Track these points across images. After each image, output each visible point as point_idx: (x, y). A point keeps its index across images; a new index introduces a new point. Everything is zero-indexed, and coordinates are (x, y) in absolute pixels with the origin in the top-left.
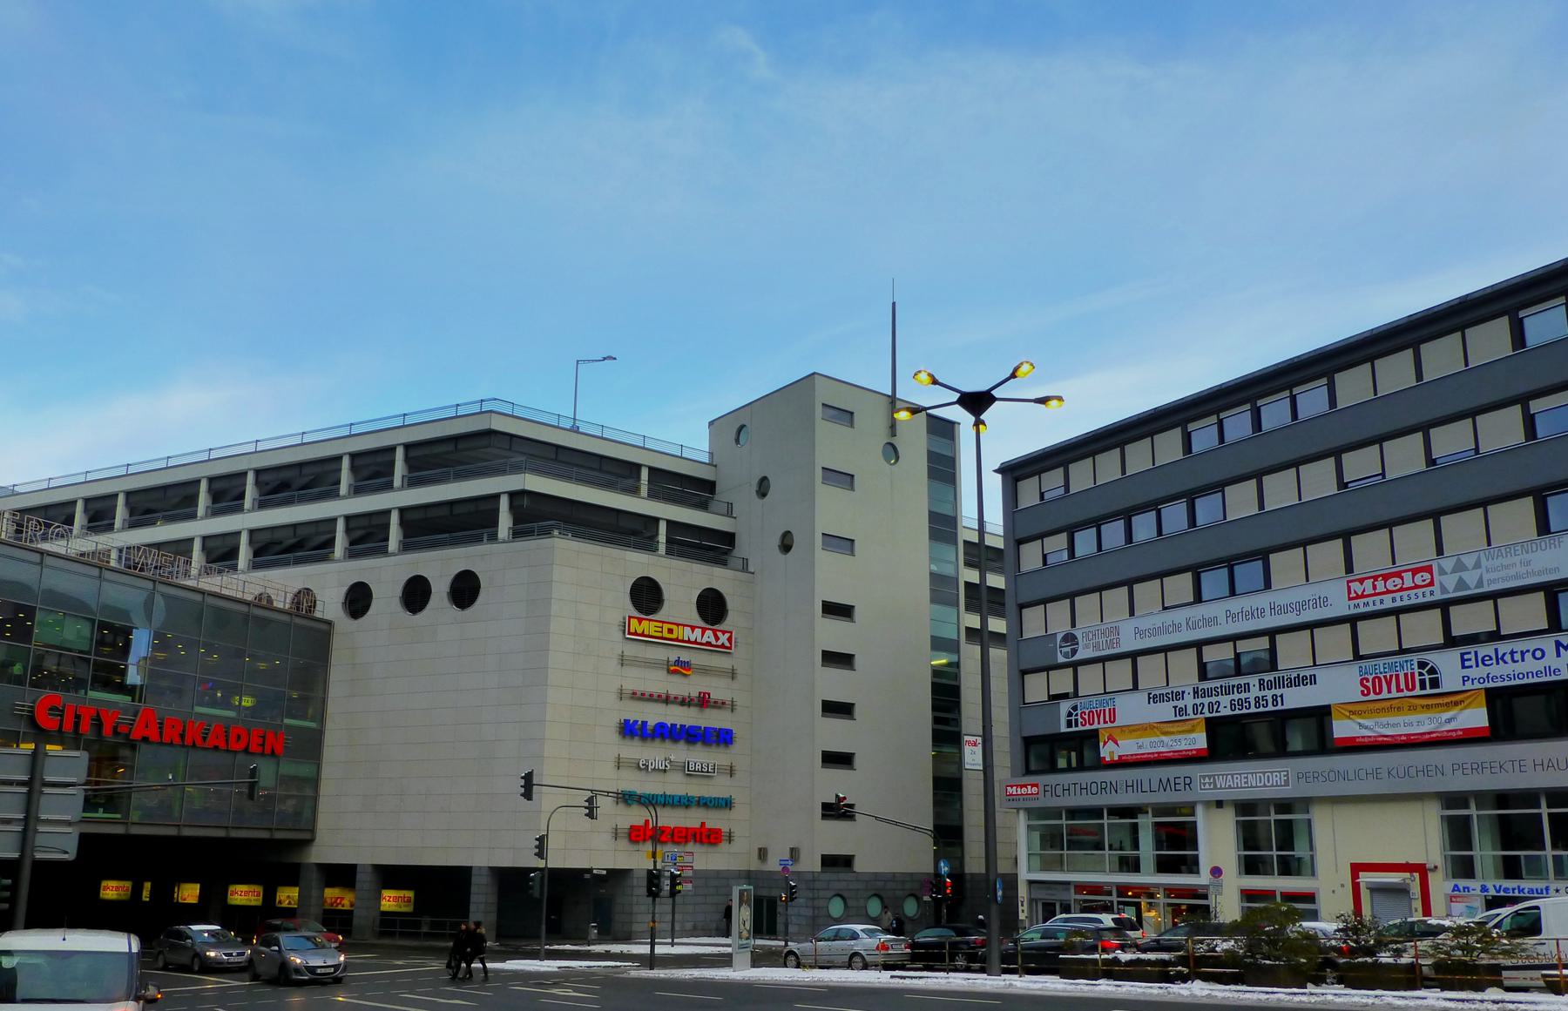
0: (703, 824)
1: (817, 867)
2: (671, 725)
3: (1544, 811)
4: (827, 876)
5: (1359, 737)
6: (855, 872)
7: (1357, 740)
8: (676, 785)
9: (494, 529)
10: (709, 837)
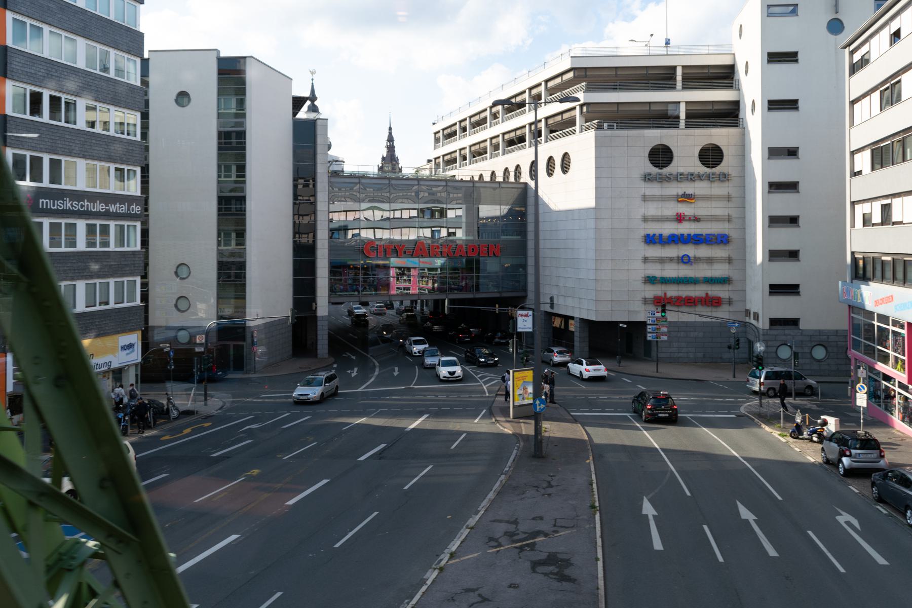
0: (707, 294)
1: (767, 326)
2: (688, 235)
3: (487, 395)
4: (774, 332)
5: (316, 304)
6: (800, 330)
7: (314, 304)
8: (672, 271)
9: (143, 179)
10: (715, 302)
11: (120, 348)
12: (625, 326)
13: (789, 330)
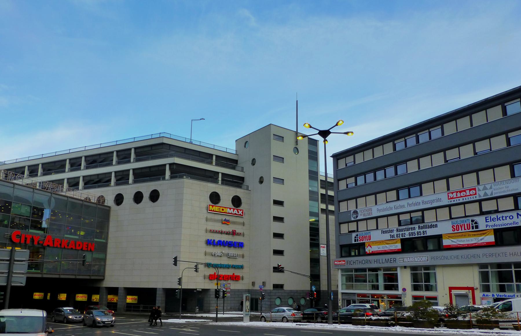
0: (234, 274)
1: (272, 288)
4: (275, 291)
6: (284, 290)
8: (225, 261)
10: (236, 278)
11: (493, 294)
12: (49, 294)
13: (280, 291)
